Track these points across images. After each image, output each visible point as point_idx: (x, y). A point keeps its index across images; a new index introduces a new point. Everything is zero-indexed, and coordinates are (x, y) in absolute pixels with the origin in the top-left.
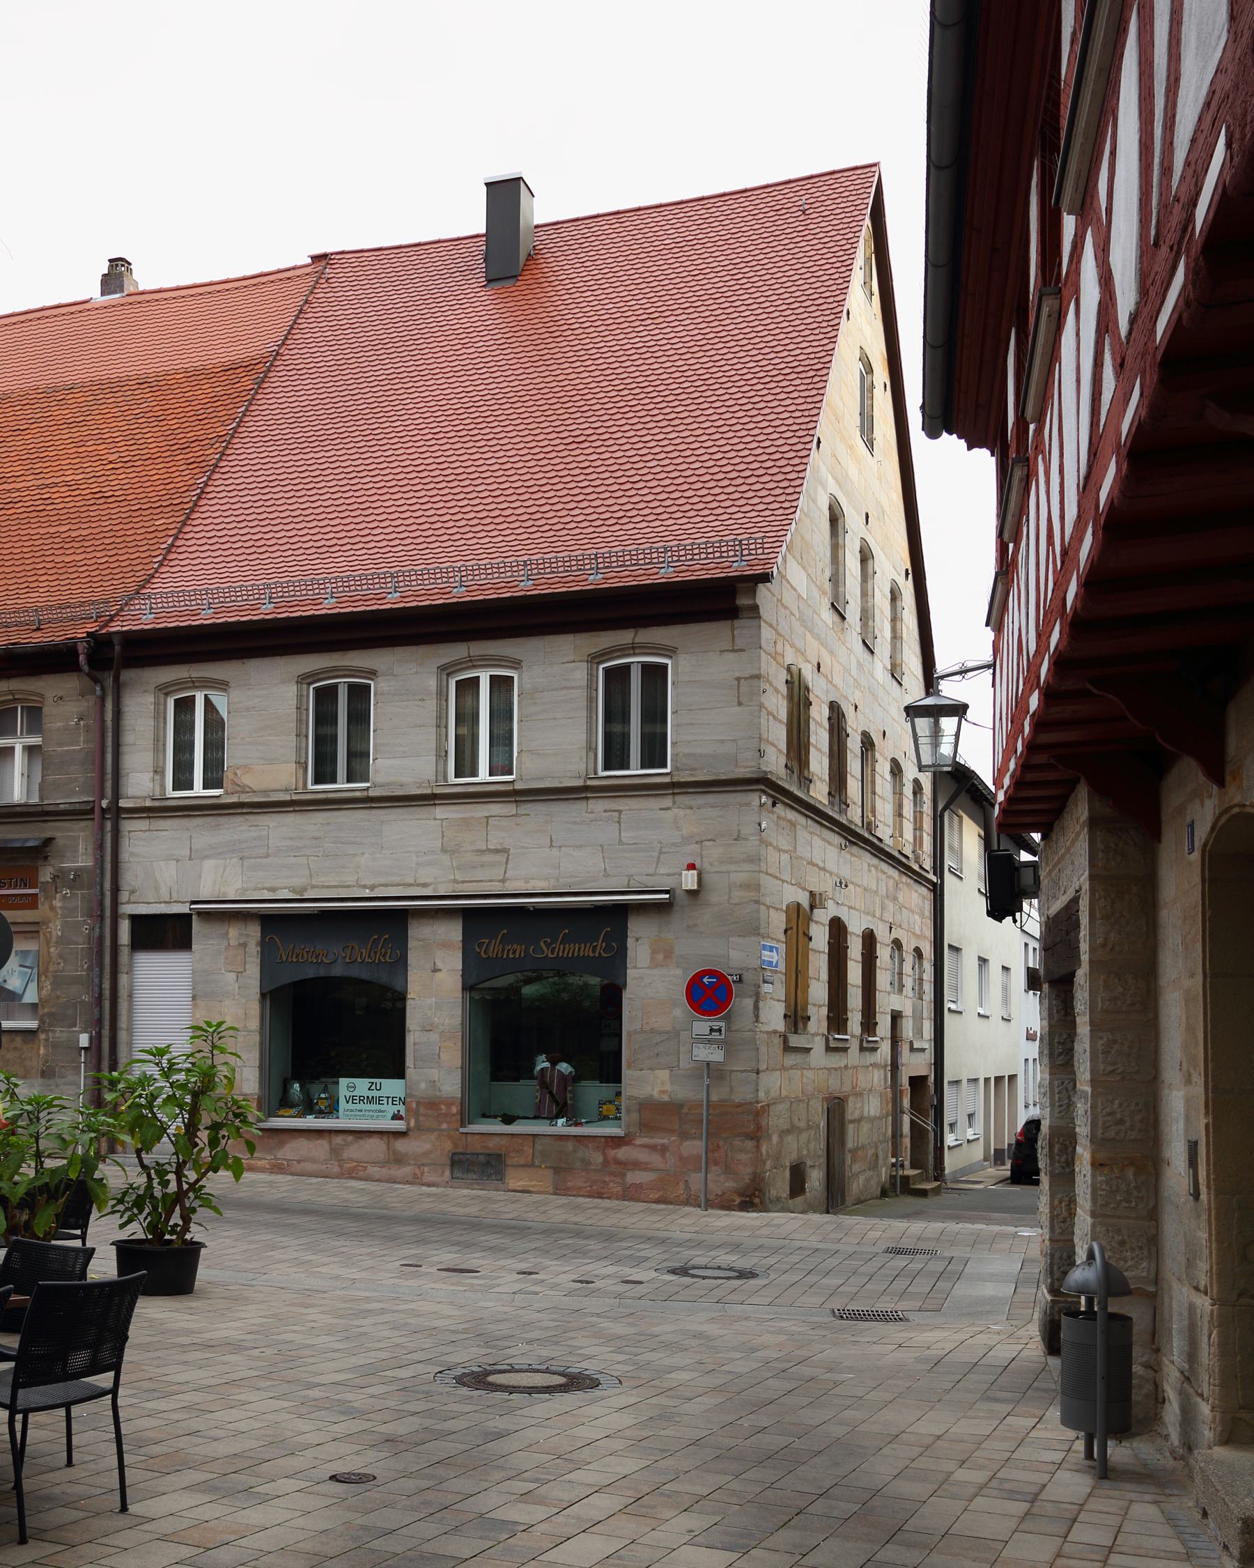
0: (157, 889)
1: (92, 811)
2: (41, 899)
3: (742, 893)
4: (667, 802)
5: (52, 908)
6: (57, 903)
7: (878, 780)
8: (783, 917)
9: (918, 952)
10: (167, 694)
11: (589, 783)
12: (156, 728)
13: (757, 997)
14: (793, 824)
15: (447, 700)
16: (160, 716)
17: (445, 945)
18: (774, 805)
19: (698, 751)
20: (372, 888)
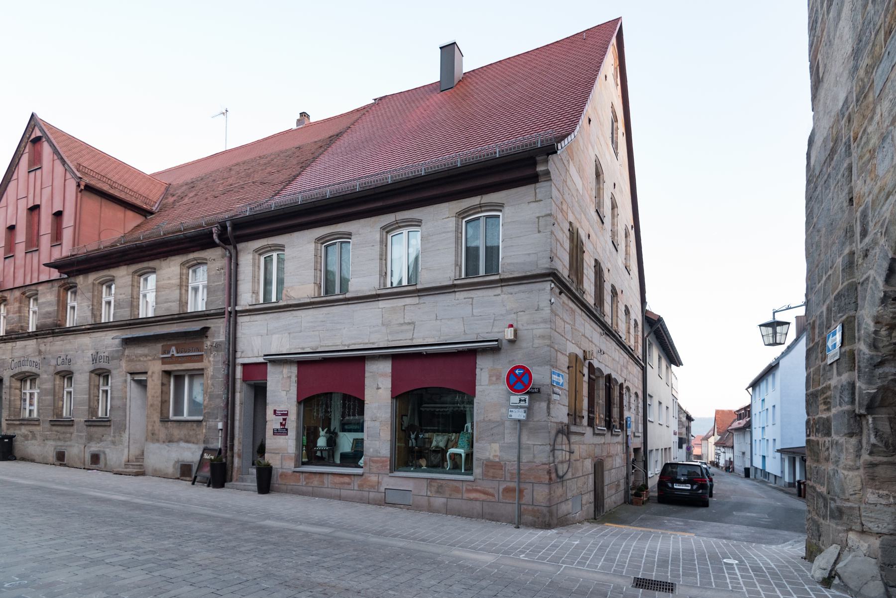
0: (252, 350)
1: (224, 313)
2: (205, 356)
3: (540, 341)
4: (498, 291)
5: (209, 361)
6: (211, 359)
7: (619, 322)
8: (567, 359)
9: (636, 393)
10: (260, 254)
11: (456, 282)
12: (254, 271)
13: (549, 402)
14: (573, 311)
15: (386, 246)
16: (255, 265)
17: (383, 375)
18: (560, 293)
19: (515, 261)
20: (348, 346)
